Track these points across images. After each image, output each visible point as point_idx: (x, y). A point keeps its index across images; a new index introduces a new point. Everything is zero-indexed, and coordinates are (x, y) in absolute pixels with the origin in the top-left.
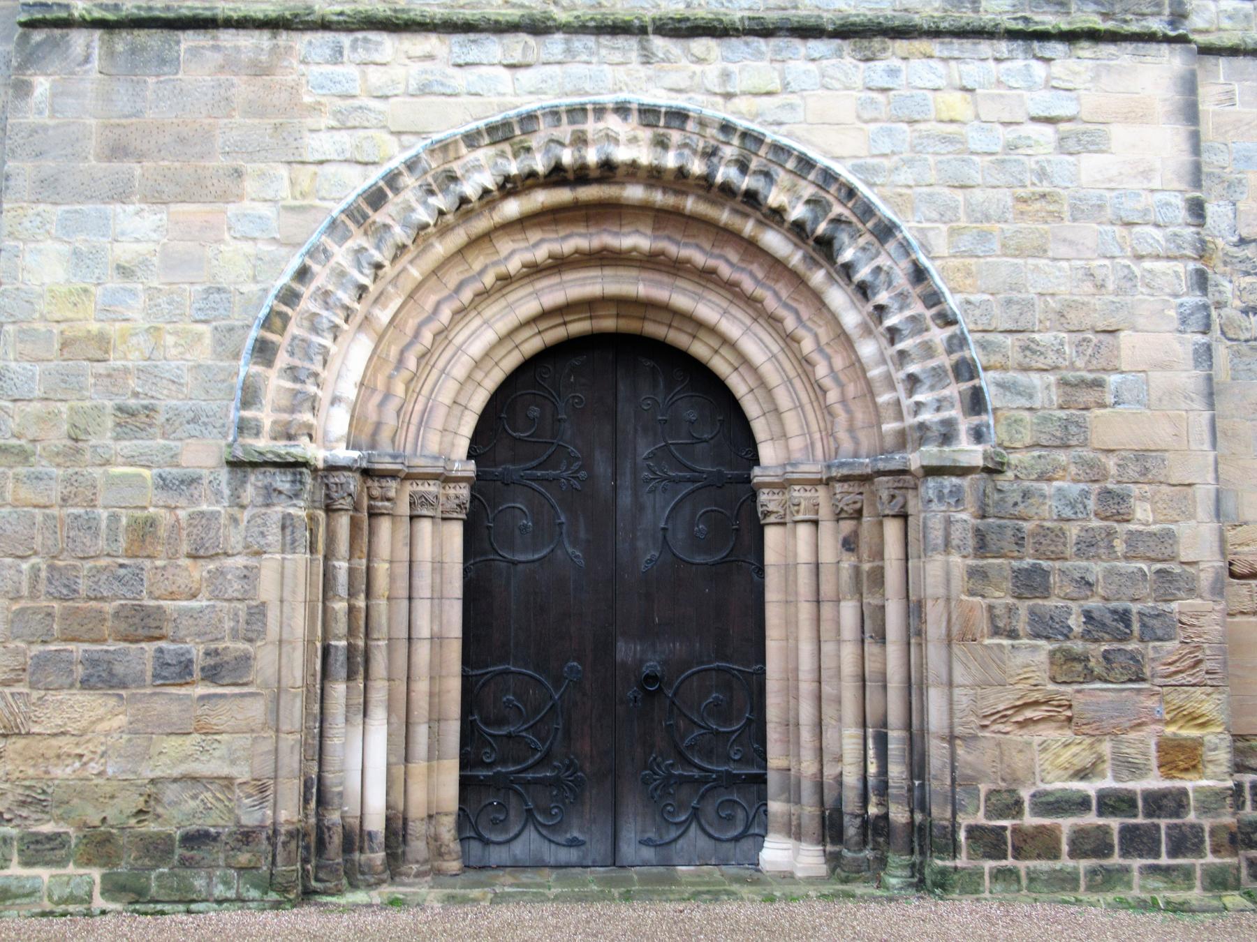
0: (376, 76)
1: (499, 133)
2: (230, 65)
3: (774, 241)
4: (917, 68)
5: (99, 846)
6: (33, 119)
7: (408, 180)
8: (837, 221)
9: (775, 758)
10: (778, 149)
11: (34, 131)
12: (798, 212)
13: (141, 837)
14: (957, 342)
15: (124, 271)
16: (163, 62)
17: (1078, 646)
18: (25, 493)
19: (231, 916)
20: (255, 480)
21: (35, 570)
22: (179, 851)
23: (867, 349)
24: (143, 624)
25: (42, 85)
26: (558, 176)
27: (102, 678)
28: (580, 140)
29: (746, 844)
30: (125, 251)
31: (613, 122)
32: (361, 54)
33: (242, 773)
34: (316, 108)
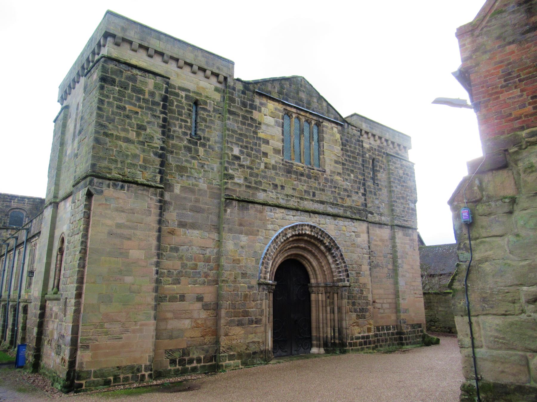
0: (276, 215)
1: (293, 228)
2: (256, 211)
3: (322, 248)
4: (341, 222)
5: (240, 356)
6: (227, 217)
7: (281, 235)
8: (332, 246)
9: (314, 334)
10: (326, 234)
11: (228, 219)
12: (327, 244)
13: (246, 353)
14: (346, 266)
15: (242, 247)
16: (247, 208)
17: (359, 314)
18: (228, 289)
19: (262, 366)
20: (262, 287)
21: (229, 303)
22: (252, 356)
23: (333, 266)
24: (246, 314)
25: (229, 211)
26: (299, 235)
27: (240, 324)
28: (302, 230)
29: (308, 350)
30: (242, 243)
31: (306, 227)
32: (274, 211)
33: (260, 340)
34: (268, 220)
